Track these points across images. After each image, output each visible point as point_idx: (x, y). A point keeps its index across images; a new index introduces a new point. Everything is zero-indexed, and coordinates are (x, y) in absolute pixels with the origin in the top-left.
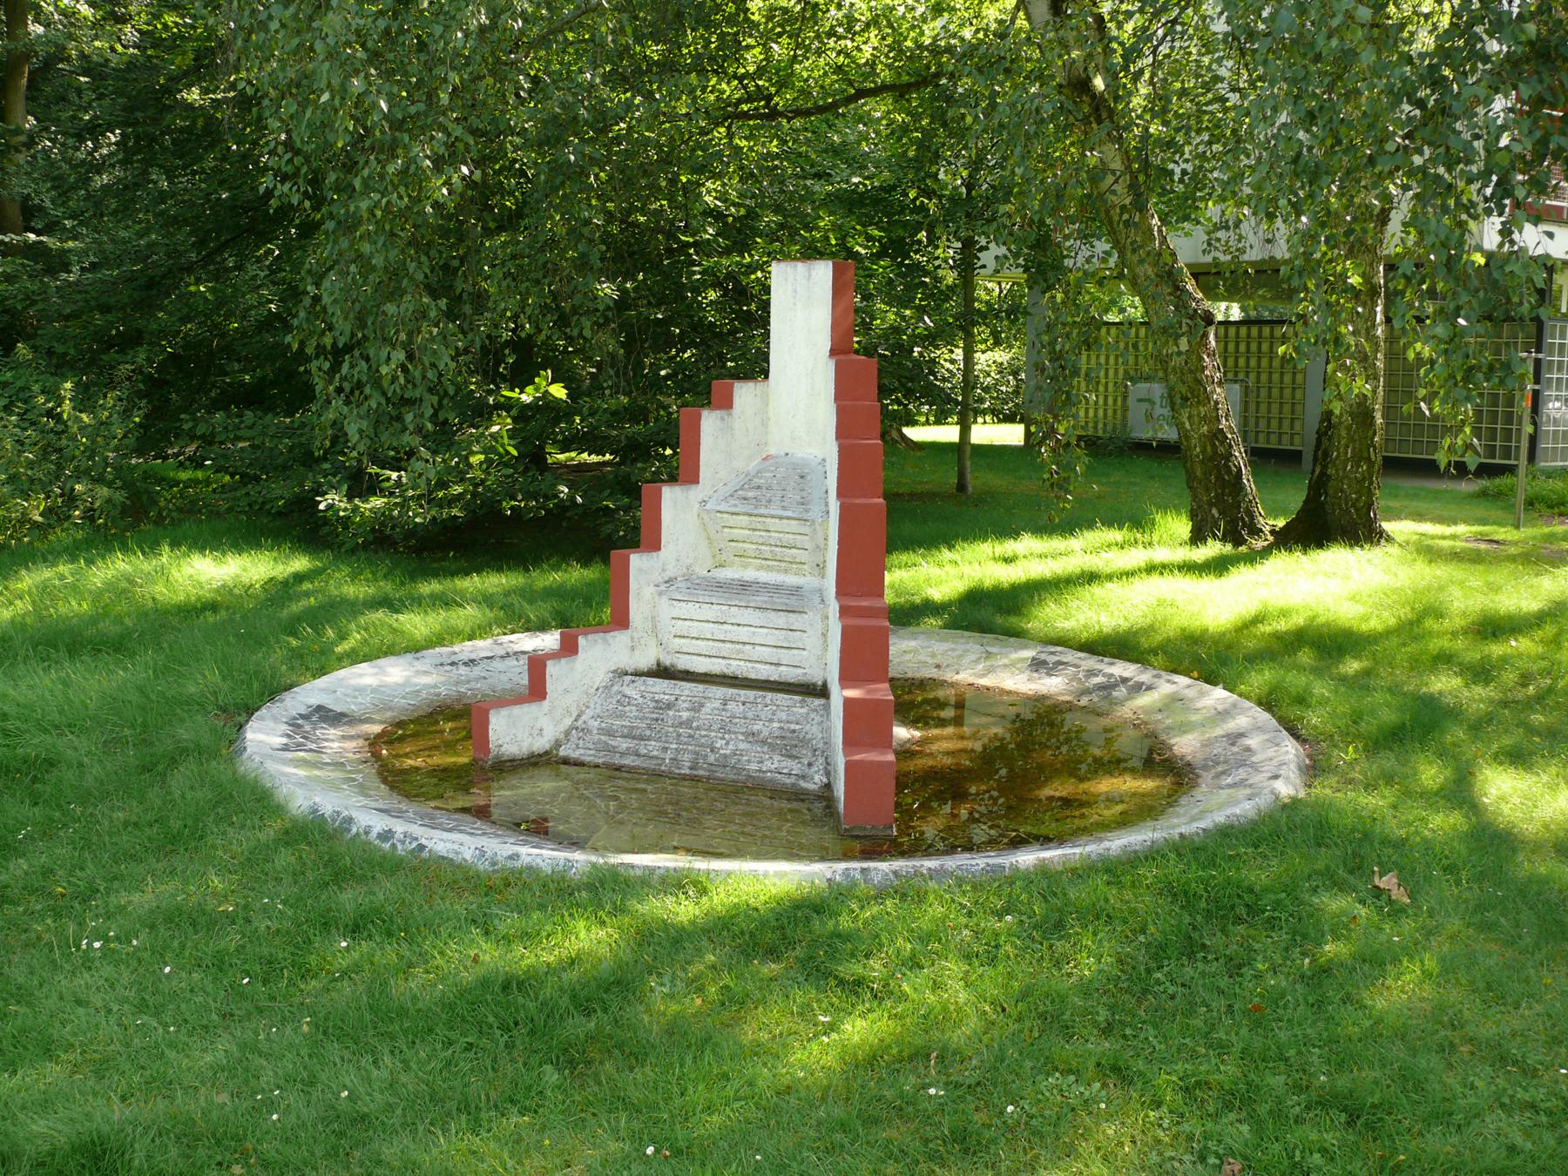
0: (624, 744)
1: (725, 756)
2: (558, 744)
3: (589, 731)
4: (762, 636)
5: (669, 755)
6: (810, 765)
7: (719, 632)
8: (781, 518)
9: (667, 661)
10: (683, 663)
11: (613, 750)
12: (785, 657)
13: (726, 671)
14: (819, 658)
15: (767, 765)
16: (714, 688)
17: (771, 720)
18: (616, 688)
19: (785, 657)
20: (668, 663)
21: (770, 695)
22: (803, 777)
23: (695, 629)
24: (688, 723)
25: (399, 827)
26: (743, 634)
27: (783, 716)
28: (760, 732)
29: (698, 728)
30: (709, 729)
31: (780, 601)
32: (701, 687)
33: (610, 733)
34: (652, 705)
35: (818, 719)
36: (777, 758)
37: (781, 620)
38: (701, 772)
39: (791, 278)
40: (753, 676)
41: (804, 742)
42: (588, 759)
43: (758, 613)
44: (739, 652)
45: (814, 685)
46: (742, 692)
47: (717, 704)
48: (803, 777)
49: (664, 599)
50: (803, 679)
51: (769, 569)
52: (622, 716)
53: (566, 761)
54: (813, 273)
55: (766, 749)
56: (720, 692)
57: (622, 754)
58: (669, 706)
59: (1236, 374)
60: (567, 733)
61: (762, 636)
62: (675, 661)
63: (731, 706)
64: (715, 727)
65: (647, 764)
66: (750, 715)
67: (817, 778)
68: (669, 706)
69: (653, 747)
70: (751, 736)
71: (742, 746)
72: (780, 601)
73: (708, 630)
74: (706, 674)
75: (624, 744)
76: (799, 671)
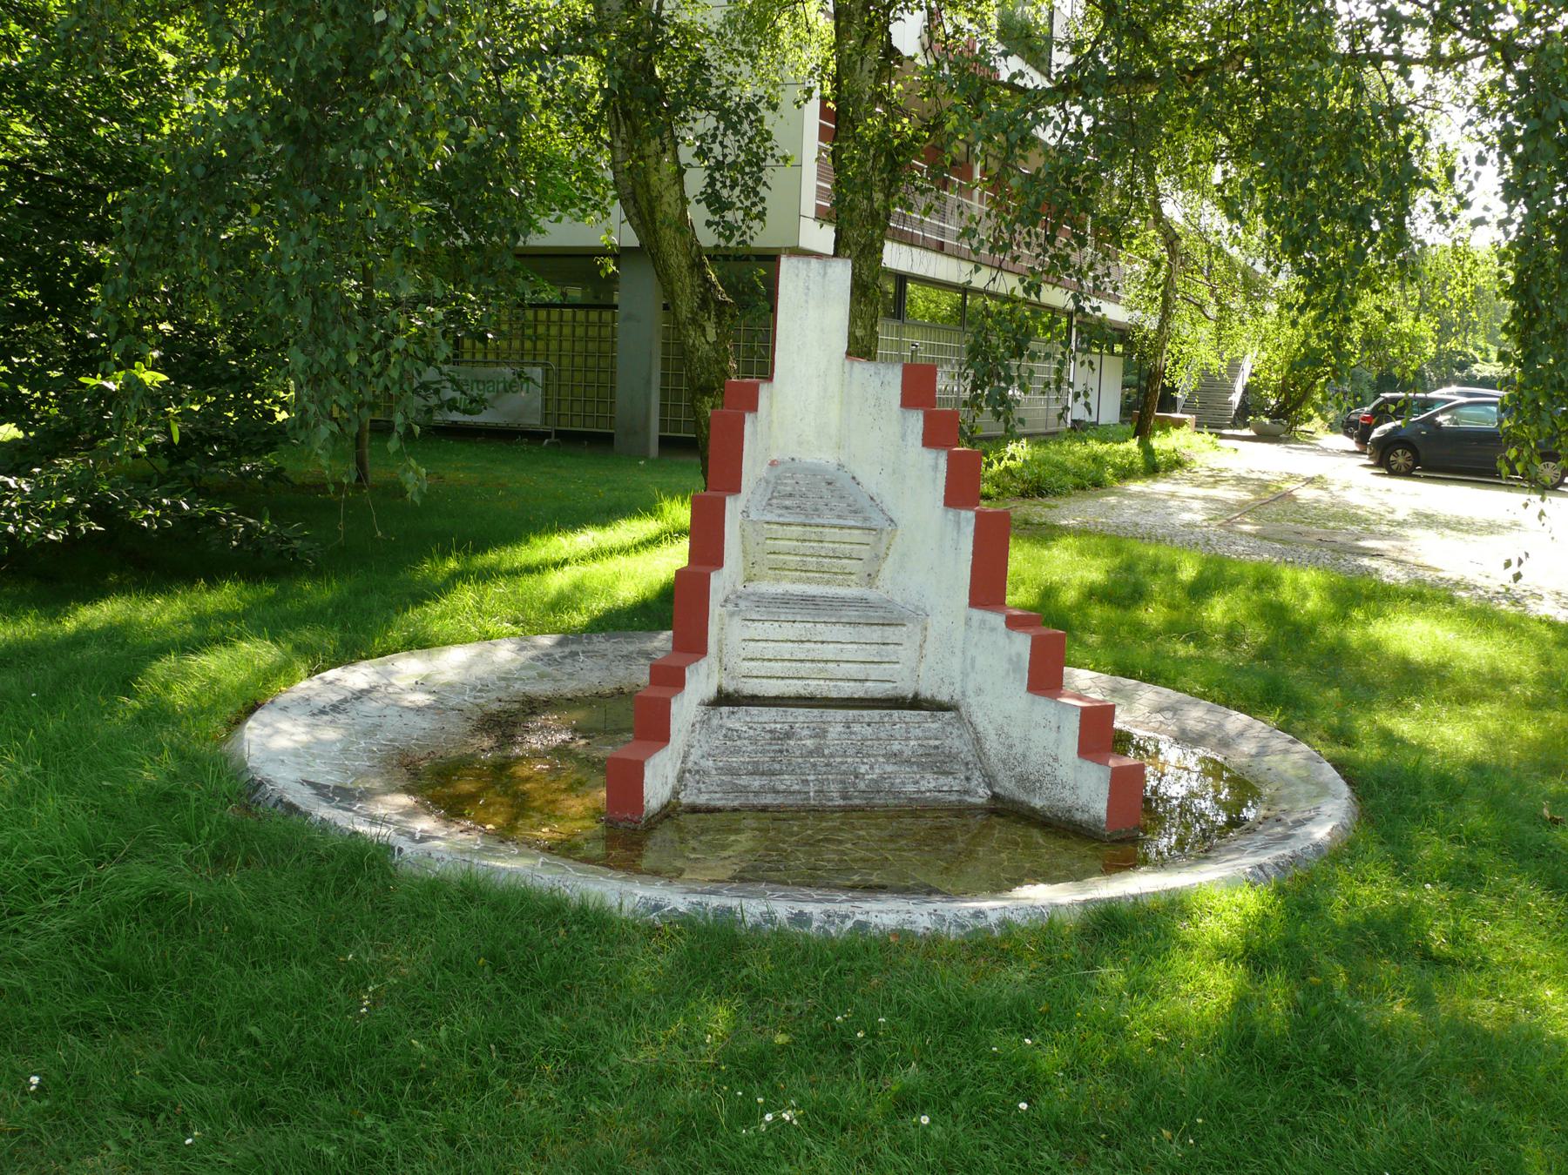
0: (756, 783)
1: (876, 781)
2: (676, 793)
3: (706, 773)
4: (850, 652)
5: (812, 788)
6: (968, 779)
7: (799, 651)
8: (842, 528)
9: (730, 687)
10: (751, 687)
11: (744, 790)
12: (875, 672)
13: (803, 692)
14: (913, 670)
15: (924, 785)
16: (832, 712)
17: (908, 739)
18: (715, 722)
19: (875, 672)
20: (731, 690)
21: (896, 713)
22: (966, 792)
23: (770, 650)
24: (818, 751)
25: (814, 909)
26: (829, 651)
27: (918, 732)
28: (901, 752)
29: (832, 756)
30: (845, 755)
31: (852, 614)
32: (816, 712)
33: (732, 772)
34: (768, 736)
35: (955, 732)
36: (929, 776)
37: (875, 634)
38: (857, 802)
39: (803, 274)
40: (834, 695)
41: (953, 757)
42: (719, 803)
43: (849, 629)
44: (821, 670)
45: (904, 698)
46: (865, 712)
47: (839, 728)
48: (966, 792)
49: (737, 620)
50: (891, 693)
51: (809, 581)
52: (737, 751)
53: (694, 809)
54: (830, 271)
55: (915, 768)
56: (840, 714)
57: (756, 793)
58: (788, 735)
59: (485, 355)
60: (680, 779)
61: (850, 652)
62: (741, 686)
63: (856, 728)
64: (851, 752)
65: (790, 800)
66: (882, 735)
67: (981, 791)
68: (788, 735)
69: (787, 781)
70: (893, 756)
71: (889, 768)
72: (875, 615)
73: (786, 650)
74: (776, 698)
75: (756, 783)
76: (888, 685)
